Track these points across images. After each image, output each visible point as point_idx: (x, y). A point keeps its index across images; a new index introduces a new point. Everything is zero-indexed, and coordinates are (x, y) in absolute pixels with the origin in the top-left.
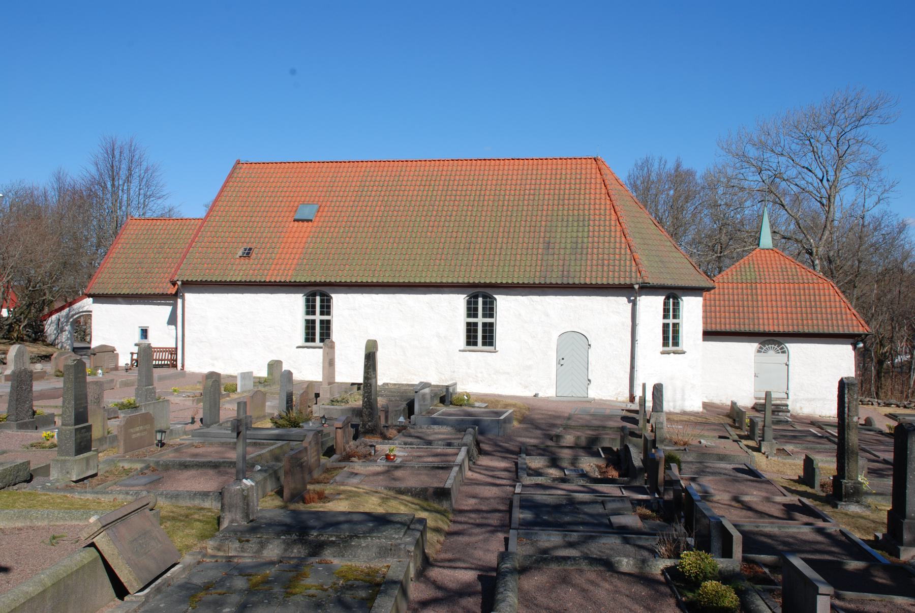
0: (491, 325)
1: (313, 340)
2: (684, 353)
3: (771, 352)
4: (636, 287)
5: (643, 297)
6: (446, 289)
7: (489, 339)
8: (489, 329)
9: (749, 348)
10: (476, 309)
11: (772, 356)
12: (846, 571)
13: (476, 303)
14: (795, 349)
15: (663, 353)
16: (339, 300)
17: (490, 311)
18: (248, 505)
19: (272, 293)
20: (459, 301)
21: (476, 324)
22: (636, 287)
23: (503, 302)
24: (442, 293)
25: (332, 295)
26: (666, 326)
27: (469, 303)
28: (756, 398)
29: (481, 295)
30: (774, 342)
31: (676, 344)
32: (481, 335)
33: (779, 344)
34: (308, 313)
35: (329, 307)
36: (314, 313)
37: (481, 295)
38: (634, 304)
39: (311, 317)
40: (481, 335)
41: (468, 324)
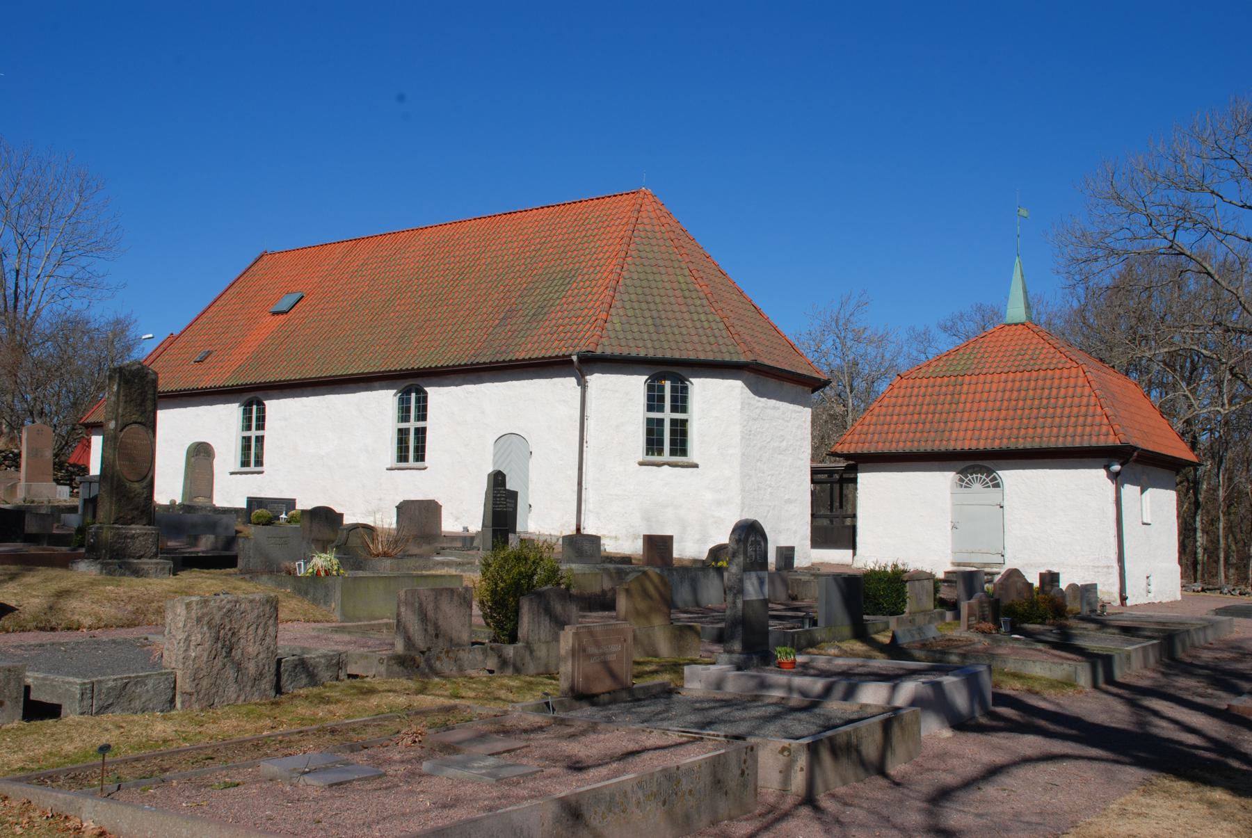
0: (684, 422)
1: (660, 452)
2: (696, 466)
3: (977, 486)
4: (575, 358)
5: (596, 375)
6: (377, 384)
7: (680, 445)
8: (680, 430)
9: (941, 482)
10: (661, 399)
11: (978, 490)
12: (398, 529)
13: (409, 401)
14: (1011, 477)
15: (641, 464)
16: (274, 407)
17: (680, 403)
18: (1059, 682)
19: (211, 404)
20: (636, 385)
21: (661, 422)
22: (575, 358)
23: (438, 396)
24: (371, 390)
25: (426, 389)
26: (403, 434)
27: (650, 388)
28: (954, 564)
29: (669, 375)
30: (982, 470)
31: (684, 452)
32: (667, 440)
33: (989, 471)
34: (650, 408)
35: (684, 399)
36: (674, 422)
37: (669, 375)
38: (583, 385)
39: (404, 425)
40: (667, 440)
41: (649, 421)
